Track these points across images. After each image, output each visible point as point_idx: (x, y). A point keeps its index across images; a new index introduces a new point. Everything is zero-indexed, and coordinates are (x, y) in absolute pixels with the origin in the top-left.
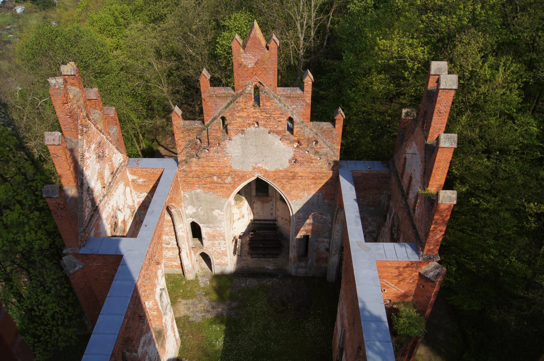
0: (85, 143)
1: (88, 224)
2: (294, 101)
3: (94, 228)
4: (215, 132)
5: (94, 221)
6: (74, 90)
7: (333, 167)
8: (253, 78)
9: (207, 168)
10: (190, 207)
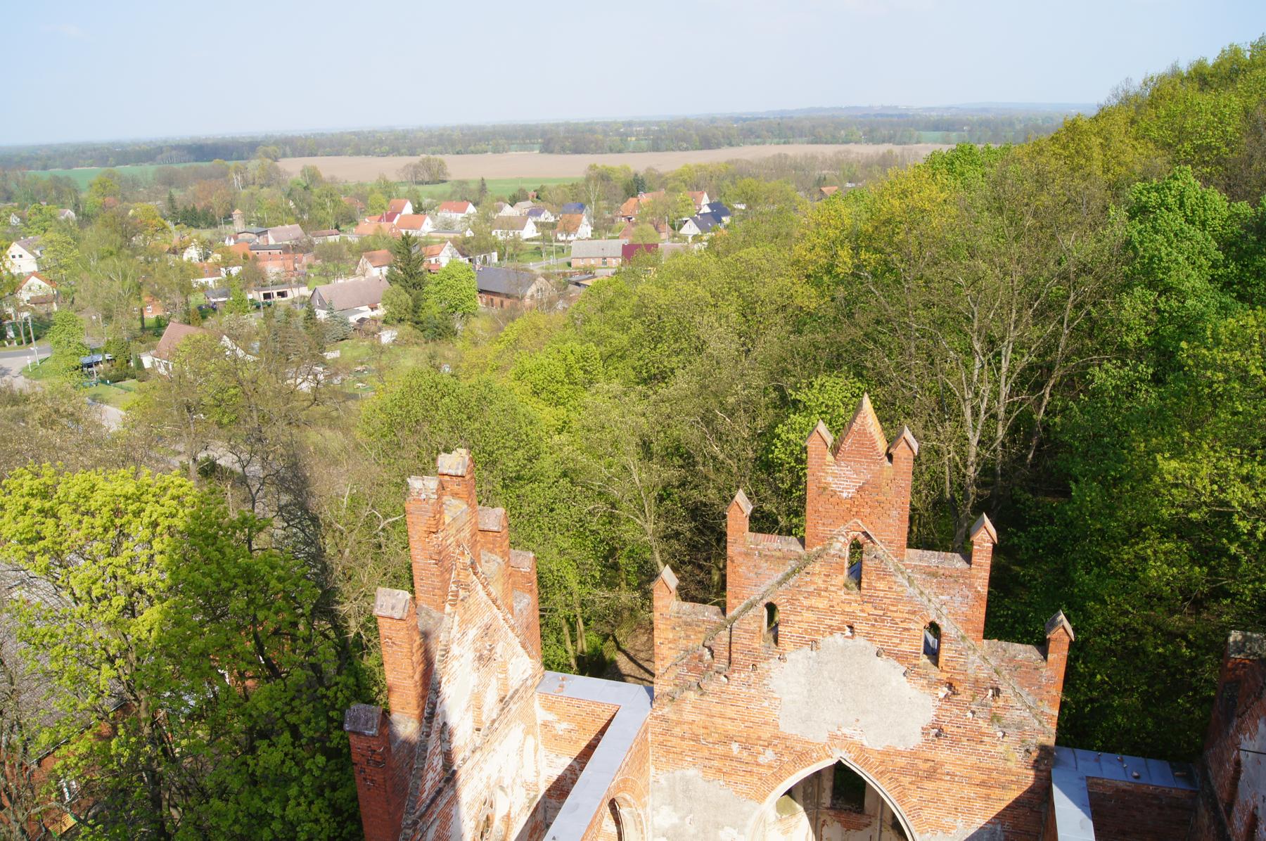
0: (456, 623)
1: (426, 810)
2: (946, 586)
3: (438, 823)
4: (747, 636)
5: (442, 806)
6: (456, 507)
7: (1036, 761)
8: (851, 523)
9: (720, 721)
10: (666, 810)
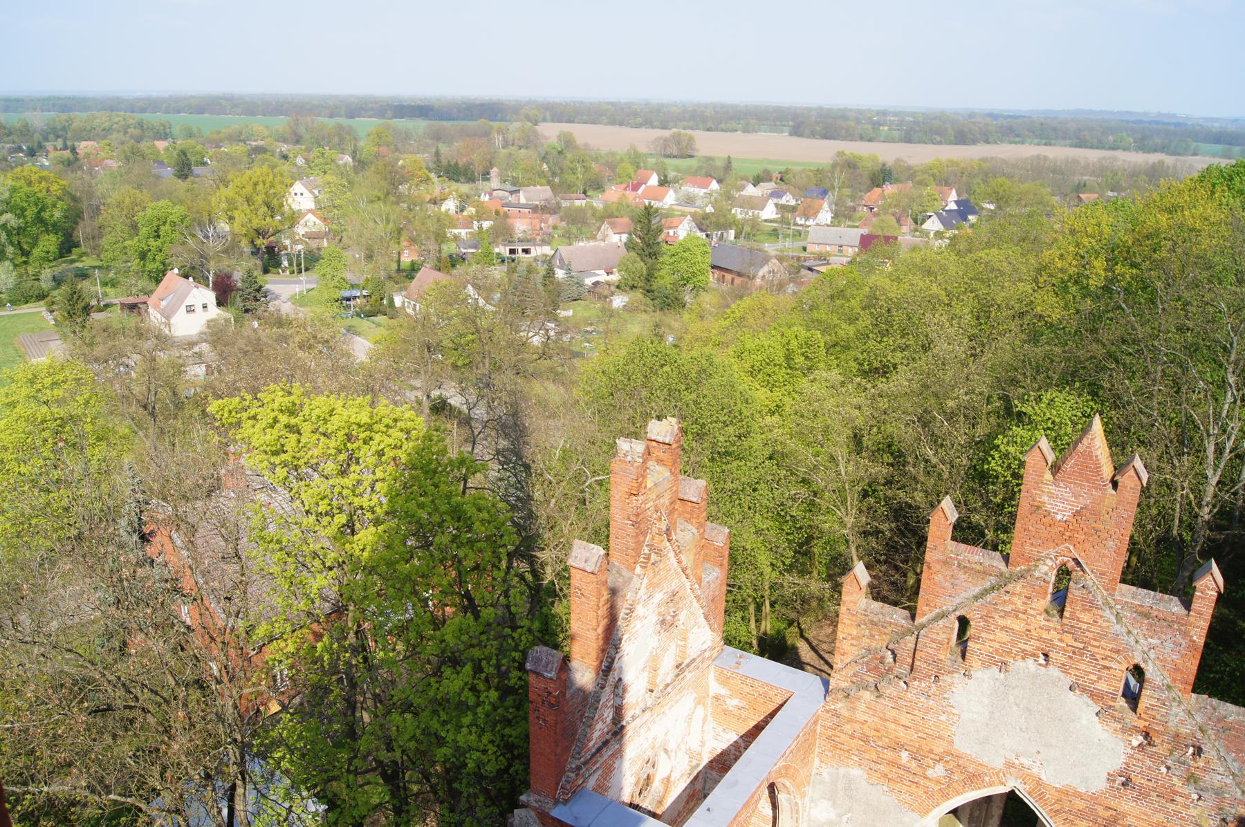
3: (600, 772)
4: (934, 645)
5: (606, 757)
6: (659, 473)
9: (893, 726)
